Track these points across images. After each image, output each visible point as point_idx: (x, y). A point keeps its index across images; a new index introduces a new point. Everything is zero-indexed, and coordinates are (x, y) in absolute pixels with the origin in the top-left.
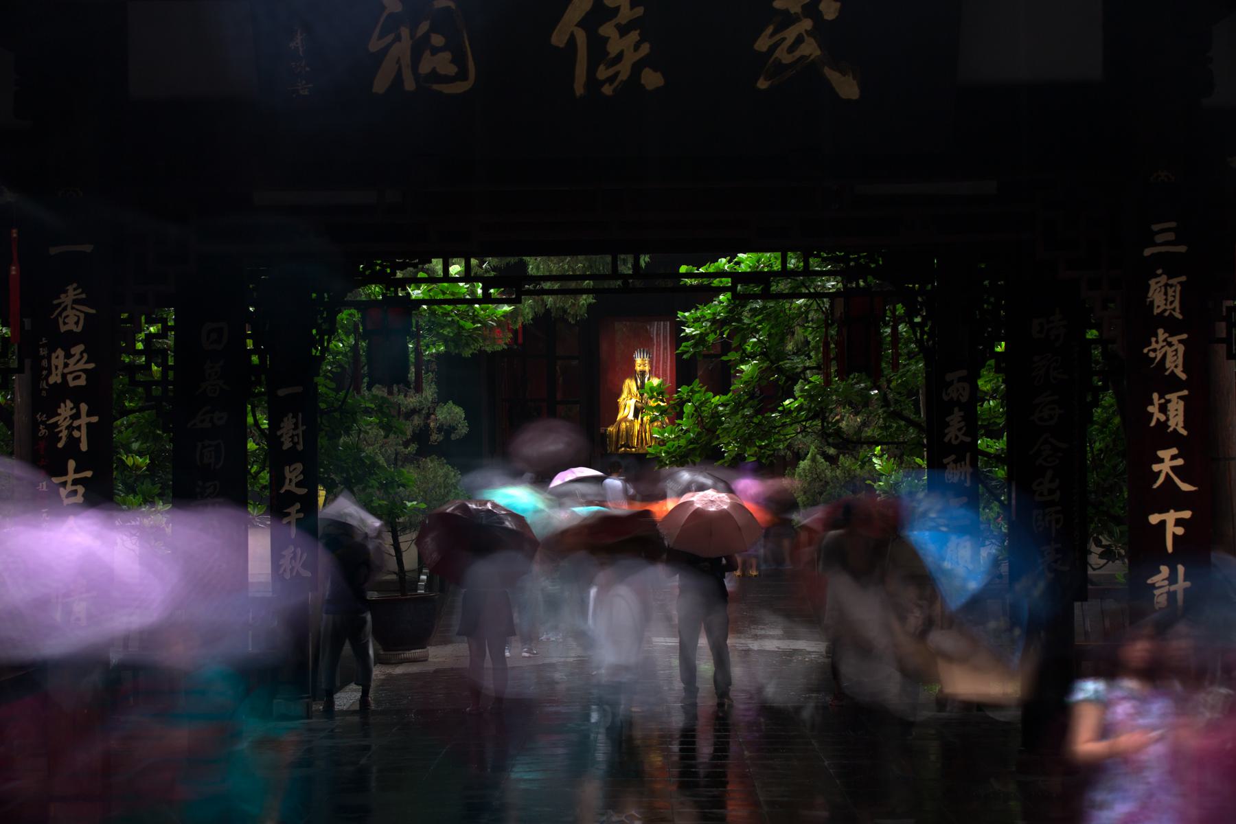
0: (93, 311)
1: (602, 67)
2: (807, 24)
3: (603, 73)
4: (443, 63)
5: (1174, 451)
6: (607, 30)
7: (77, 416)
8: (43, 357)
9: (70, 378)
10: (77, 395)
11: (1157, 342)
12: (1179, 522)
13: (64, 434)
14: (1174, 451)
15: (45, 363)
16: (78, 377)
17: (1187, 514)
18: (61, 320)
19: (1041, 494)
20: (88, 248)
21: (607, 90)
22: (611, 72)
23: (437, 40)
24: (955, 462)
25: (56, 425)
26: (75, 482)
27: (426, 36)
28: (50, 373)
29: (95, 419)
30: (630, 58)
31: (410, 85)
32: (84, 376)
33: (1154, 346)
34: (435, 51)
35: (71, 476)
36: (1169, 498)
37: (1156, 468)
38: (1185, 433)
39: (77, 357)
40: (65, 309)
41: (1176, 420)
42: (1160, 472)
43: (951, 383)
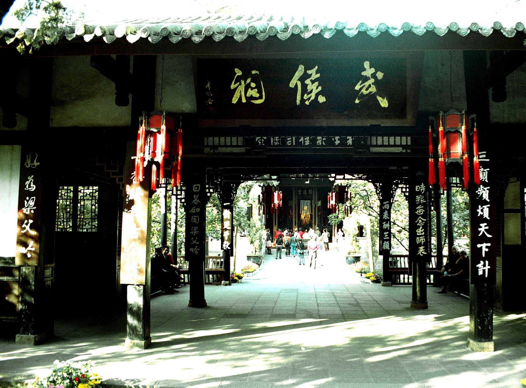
1: (306, 95)
2: (372, 81)
4: (254, 93)
5: (486, 224)
6: (308, 82)
12: (487, 247)
14: (486, 224)
17: (489, 245)
21: (307, 103)
23: (253, 85)
27: (249, 84)
31: (244, 101)
33: (479, 190)
34: (252, 89)
37: (479, 229)
38: (489, 218)
41: (486, 215)
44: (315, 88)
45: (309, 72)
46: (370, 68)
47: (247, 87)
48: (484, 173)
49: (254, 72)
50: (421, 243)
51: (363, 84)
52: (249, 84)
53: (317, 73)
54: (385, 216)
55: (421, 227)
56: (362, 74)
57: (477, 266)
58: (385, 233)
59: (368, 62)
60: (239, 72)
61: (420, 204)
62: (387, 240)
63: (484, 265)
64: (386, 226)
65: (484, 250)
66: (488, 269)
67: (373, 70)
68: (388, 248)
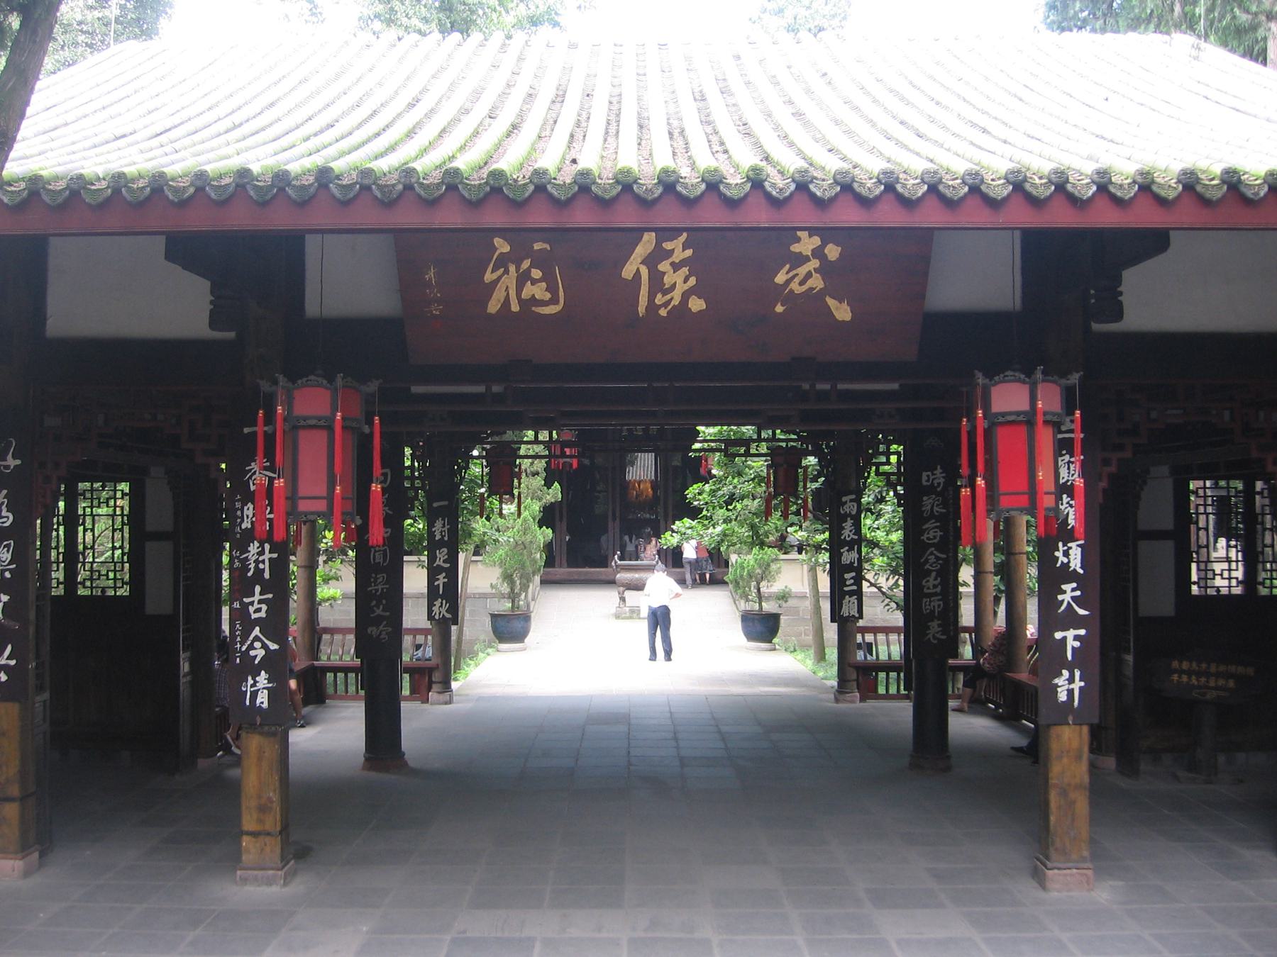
1: (659, 296)
2: (814, 264)
5: (1074, 585)
6: (664, 266)
7: (261, 553)
12: (1076, 638)
13: (252, 566)
14: (1074, 585)
15: (239, 513)
17: (1082, 632)
21: (663, 312)
22: (668, 297)
23: (536, 274)
26: (260, 602)
27: (528, 271)
29: (275, 555)
31: (515, 307)
34: (534, 282)
35: (257, 597)
37: (1060, 597)
41: (1076, 562)
44: (679, 281)
45: (668, 246)
48: (1072, 467)
49: (537, 246)
51: (794, 272)
52: (528, 271)
55: (934, 574)
58: (846, 576)
60: (502, 246)
61: (932, 516)
62: (851, 593)
63: (1071, 680)
64: (848, 557)
65: (1072, 644)
66: (1081, 688)
68: (855, 612)
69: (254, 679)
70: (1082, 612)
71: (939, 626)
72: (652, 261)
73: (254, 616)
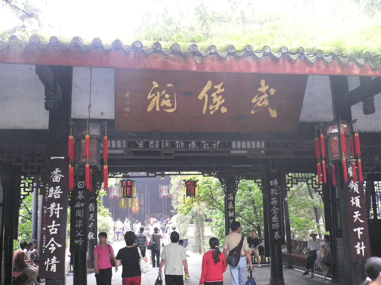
0: (63, 176)
1: (211, 106)
2: (266, 96)
3: (211, 107)
4: (167, 103)
5: (358, 212)
6: (214, 95)
7: (56, 207)
8: (47, 189)
9: (55, 196)
10: (57, 201)
11: (351, 184)
12: (361, 231)
13: (52, 213)
14: (358, 212)
15: (47, 191)
16: (57, 196)
17: (363, 228)
18: (53, 179)
19: (274, 220)
20: (63, 158)
21: (212, 113)
22: (214, 107)
23: (167, 96)
24: (231, 212)
25: (50, 210)
26: (55, 227)
27: (164, 94)
28: (49, 194)
29: (62, 208)
30: (219, 103)
31: (158, 109)
32: (59, 195)
33: (351, 185)
34: (166, 99)
35: (53, 225)
36: (358, 225)
37: (354, 216)
38: (360, 207)
39: (58, 190)
40: (55, 175)
41: (358, 204)
42: (355, 218)
43: (230, 196)
45: (216, 87)
46: (265, 85)
47: (162, 98)
49: (169, 85)
50: (276, 228)
53: (222, 88)
54: (230, 207)
55: (276, 215)
56: (224, 89)
57: (355, 247)
58: (230, 221)
59: (264, 81)
60: (156, 85)
63: (361, 246)
65: (360, 233)
66: (364, 249)
67: (267, 87)
69: (50, 259)
70: (362, 221)
71: (278, 233)
72: (209, 93)
73: (52, 233)
